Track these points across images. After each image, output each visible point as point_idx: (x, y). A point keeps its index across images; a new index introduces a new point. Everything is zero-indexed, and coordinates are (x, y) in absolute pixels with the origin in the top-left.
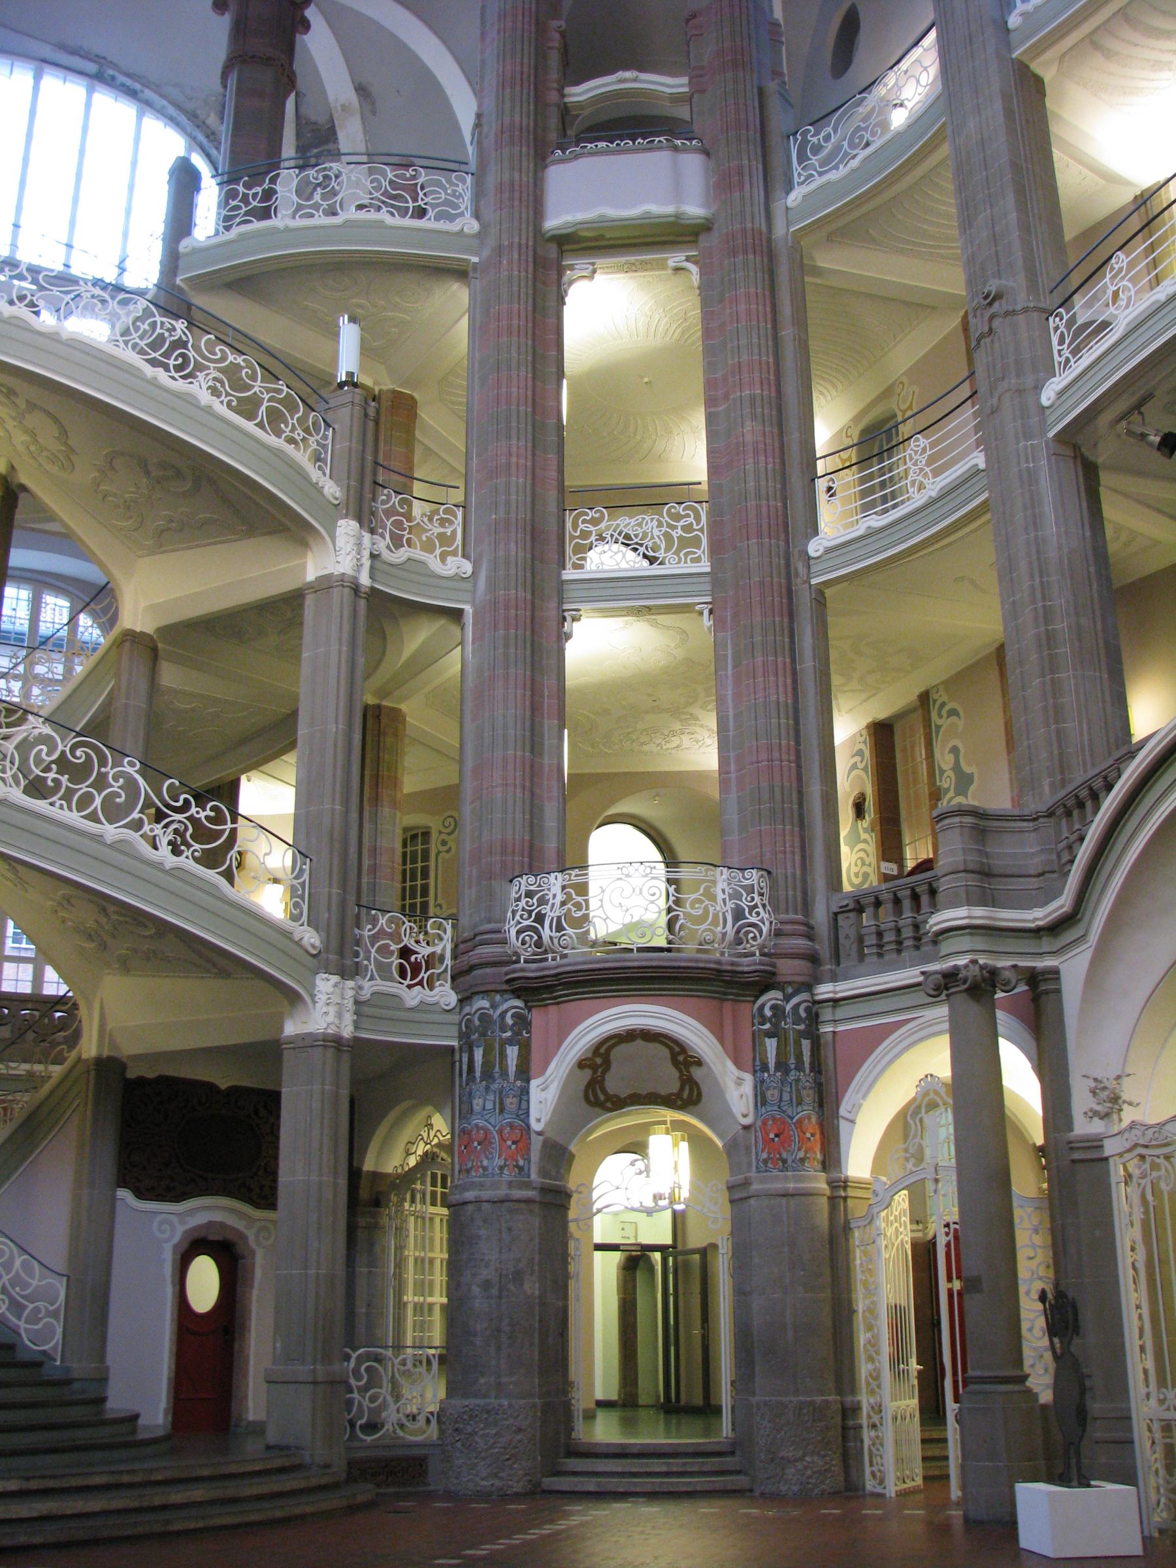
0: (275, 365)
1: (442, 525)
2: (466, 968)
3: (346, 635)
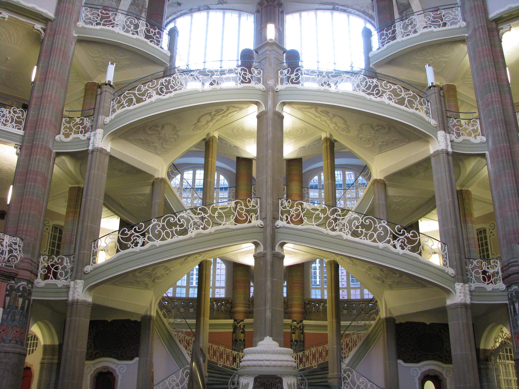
0: (407, 86)
1: (473, 126)
2: (507, 275)
3: (447, 169)
